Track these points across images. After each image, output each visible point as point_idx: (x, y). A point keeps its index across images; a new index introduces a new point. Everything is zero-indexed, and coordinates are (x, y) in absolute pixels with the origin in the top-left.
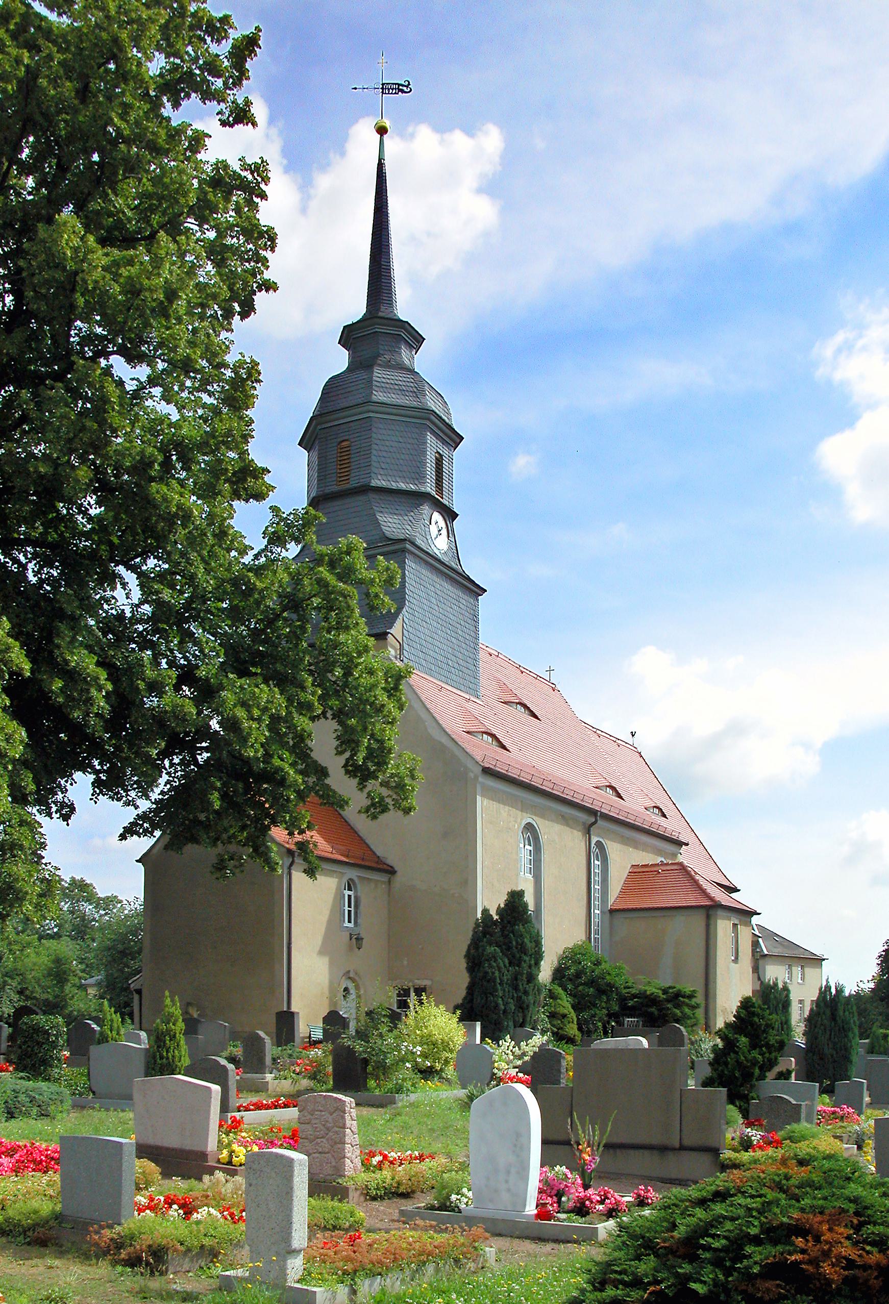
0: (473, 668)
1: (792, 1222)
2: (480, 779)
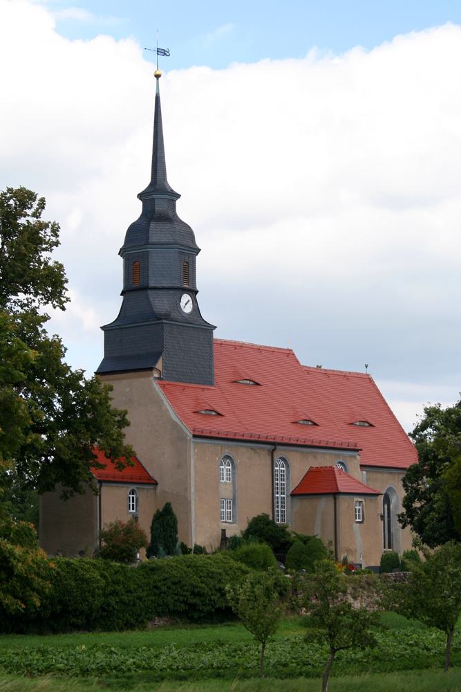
0: (208, 370)
1: (410, 663)
2: (192, 440)
